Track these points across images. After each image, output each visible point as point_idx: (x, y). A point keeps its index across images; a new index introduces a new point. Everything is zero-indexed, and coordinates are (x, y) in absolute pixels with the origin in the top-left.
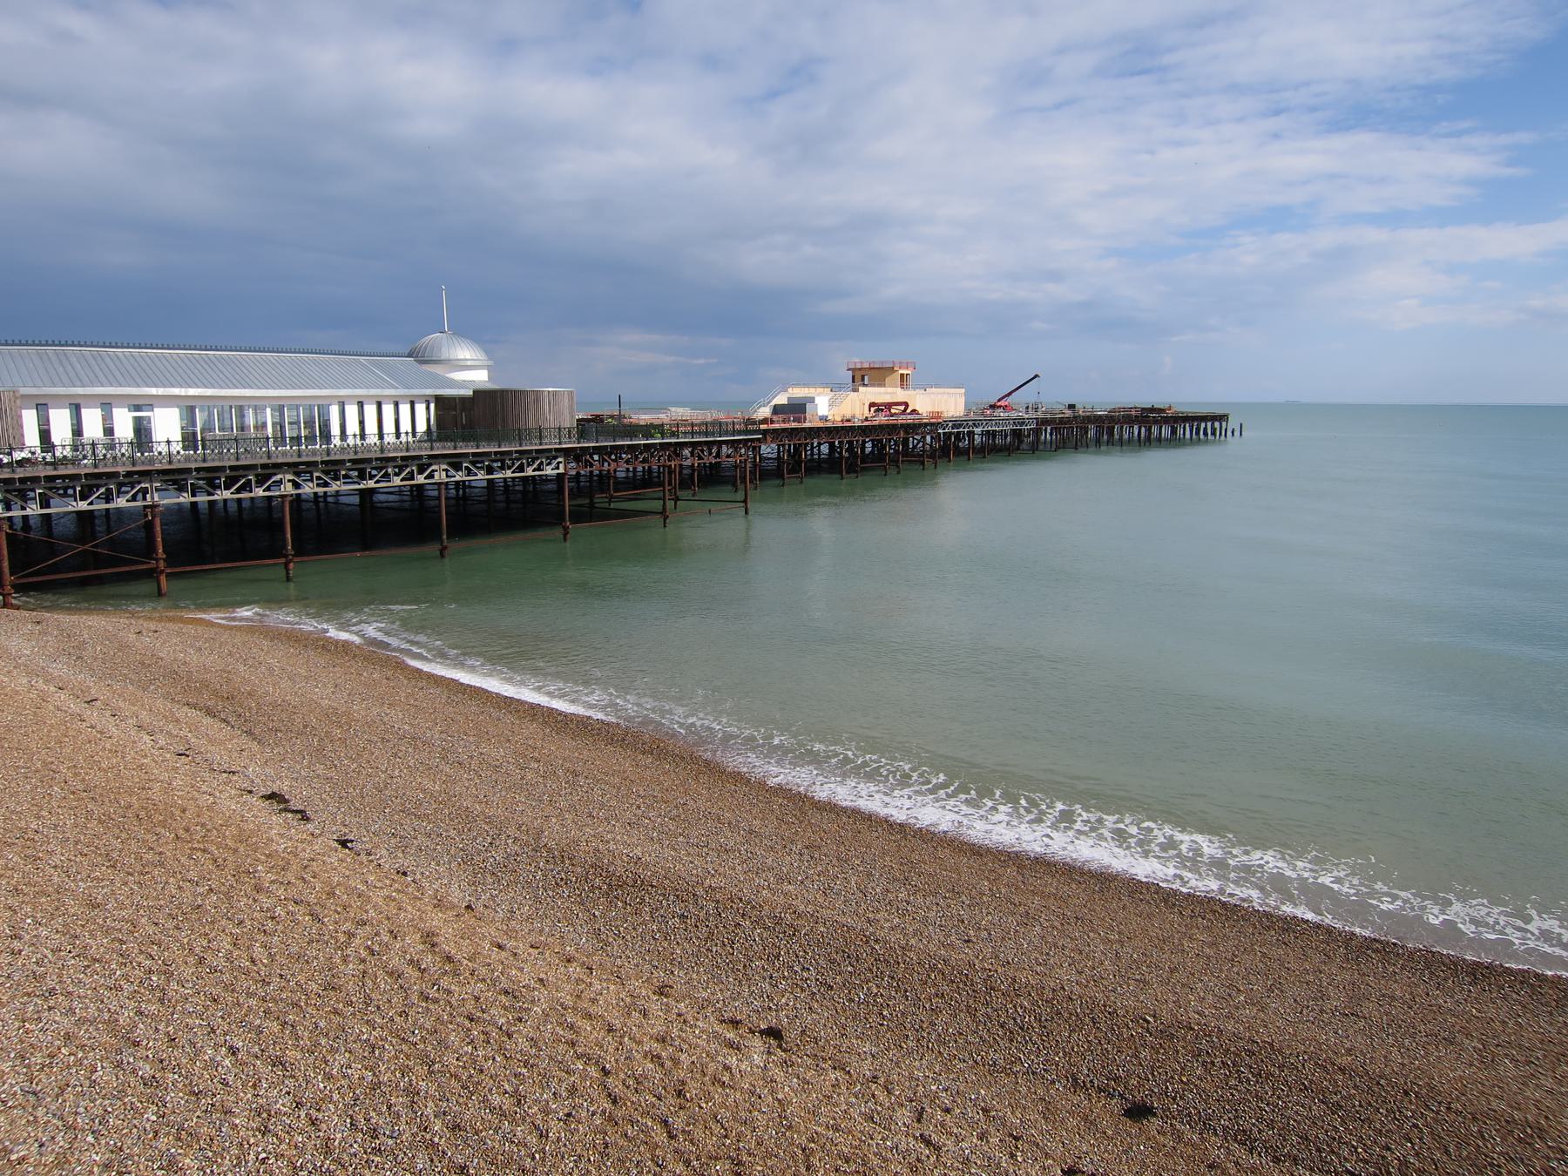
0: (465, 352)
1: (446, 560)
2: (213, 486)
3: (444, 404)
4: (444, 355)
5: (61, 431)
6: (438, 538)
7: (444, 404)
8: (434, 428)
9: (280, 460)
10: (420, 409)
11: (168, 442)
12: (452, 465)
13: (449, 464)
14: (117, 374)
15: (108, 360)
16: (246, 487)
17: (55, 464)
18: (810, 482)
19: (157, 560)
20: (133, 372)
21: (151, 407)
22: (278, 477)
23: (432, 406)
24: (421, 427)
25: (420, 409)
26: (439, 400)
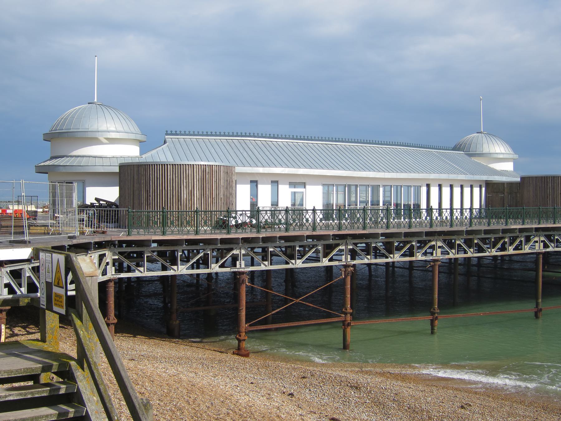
0: (499, 148)
1: (540, 321)
2: (389, 249)
3: (492, 188)
4: (486, 150)
5: (264, 202)
6: (537, 299)
7: (492, 188)
8: (484, 207)
9: (439, 229)
10: (476, 190)
11: (314, 210)
12: (548, 237)
13: (444, 241)
14: (221, 154)
15: (209, 144)
16: (205, 262)
17: (258, 227)
18: (360, 331)
19: (346, 314)
20: (273, 160)
21: (304, 185)
22: (433, 243)
23: (483, 189)
24: (476, 205)
25: (476, 190)
26: (489, 185)
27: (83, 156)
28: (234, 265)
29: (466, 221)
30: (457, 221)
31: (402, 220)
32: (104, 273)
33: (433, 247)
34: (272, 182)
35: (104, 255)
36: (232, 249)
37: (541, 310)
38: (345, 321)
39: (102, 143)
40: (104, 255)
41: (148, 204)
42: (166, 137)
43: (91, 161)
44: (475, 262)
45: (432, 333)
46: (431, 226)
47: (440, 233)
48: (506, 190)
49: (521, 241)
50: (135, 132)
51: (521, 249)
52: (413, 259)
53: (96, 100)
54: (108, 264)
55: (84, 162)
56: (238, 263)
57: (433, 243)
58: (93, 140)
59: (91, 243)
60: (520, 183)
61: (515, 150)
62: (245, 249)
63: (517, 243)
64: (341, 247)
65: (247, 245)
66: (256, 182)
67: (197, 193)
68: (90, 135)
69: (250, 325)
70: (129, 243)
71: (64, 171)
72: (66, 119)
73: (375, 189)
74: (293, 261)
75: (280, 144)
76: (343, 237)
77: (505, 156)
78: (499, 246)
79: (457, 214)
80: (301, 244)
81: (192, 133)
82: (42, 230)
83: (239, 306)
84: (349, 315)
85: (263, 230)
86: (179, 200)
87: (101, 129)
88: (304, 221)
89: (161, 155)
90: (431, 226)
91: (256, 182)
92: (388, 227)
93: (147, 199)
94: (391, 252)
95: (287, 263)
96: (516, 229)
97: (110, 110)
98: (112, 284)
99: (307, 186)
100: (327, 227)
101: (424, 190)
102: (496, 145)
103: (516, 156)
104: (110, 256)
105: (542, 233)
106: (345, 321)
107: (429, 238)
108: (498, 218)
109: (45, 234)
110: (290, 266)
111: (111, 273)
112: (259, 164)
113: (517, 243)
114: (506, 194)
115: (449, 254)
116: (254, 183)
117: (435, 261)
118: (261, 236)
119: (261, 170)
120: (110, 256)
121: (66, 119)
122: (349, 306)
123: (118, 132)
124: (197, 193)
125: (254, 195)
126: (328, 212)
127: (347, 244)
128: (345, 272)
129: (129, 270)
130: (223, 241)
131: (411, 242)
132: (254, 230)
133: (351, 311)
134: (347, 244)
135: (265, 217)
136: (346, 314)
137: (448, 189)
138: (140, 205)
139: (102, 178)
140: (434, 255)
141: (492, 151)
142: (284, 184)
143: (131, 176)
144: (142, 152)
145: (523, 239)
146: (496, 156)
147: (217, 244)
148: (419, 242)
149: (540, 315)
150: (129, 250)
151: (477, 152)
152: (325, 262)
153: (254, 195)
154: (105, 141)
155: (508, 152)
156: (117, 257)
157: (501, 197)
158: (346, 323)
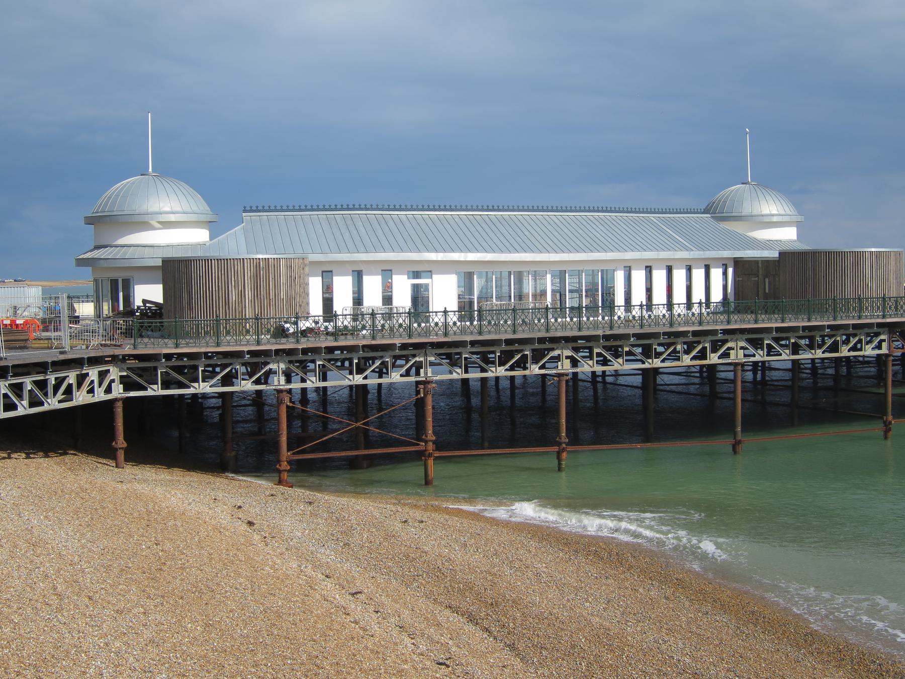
4: (747, 209)
8: (731, 297)
9: (559, 334)
10: (716, 274)
12: (751, 341)
15: (391, 224)
17: (338, 333)
19: (426, 442)
21: (429, 274)
22: (556, 353)
23: (730, 271)
24: (717, 296)
25: (716, 274)
26: (739, 264)
27: (130, 246)
28: (418, 374)
29: (693, 319)
30: (664, 321)
31: (568, 319)
32: (108, 390)
33: (558, 358)
34: (647, 267)
35: (108, 371)
36: (267, 363)
37: (740, 442)
38: (426, 450)
39: (154, 228)
40: (108, 371)
41: (191, 309)
42: (244, 214)
43: (138, 253)
44: (475, 386)
45: (886, 438)
46: (671, 325)
47: (567, 339)
48: (761, 271)
49: (704, 348)
50: (198, 211)
51: (861, 350)
52: (527, 372)
53: (150, 170)
54: (113, 381)
55: (129, 253)
56: (422, 371)
57: (556, 353)
58: (141, 224)
59: (83, 358)
60: (779, 261)
61: (797, 205)
62: (284, 362)
63: (853, 341)
64: (417, 359)
65: (570, 345)
66: (650, 267)
67: (249, 294)
68: (137, 219)
69: (294, 454)
70: (180, 356)
71: (106, 265)
72: (720, 201)
73: (520, 277)
74: (650, 361)
75: (493, 218)
76: (555, 340)
77: (786, 219)
78: (875, 343)
79: (679, 310)
80: (822, 333)
81: (315, 207)
82: (44, 344)
83: (279, 430)
84: (431, 444)
85: (343, 337)
86: (227, 302)
87: (151, 210)
88: (616, 318)
89: (236, 244)
90: (611, 328)
91: (650, 267)
92: (514, 332)
93: (190, 303)
94: (649, 357)
95: (451, 373)
96: (688, 332)
97: (172, 184)
98: (120, 405)
99: (434, 276)
100: (463, 331)
101: (620, 276)
102: (763, 202)
103: (800, 218)
104: (115, 373)
105: (741, 336)
106: (426, 450)
107: (726, 337)
108: (770, 314)
109: (48, 348)
110: (646, 366)
111: (118, 391)
112: (511, 249)
113: (853, 341)
114: (760, 276)
115: (781, 355)
116: (327, 276)
117: (559, 375)
118: (300, 347)
119: (363, 257)
120: (115, 373)
121: (720, 201)
122: (430, 432)
123: (184, 213)
124: (249, 294)
125: (328, 290)
126: (465, 308)
127: (426, 355)
128: (424, 389)
129: (182, 385)
130: (778, 329)
131: (522, 351)
132: (330, 338)
133: (434, 438)
134: (426, 355)
135: (345, 322)
136: (426, 442)
137: (702, 272)
138: (182, 309)
139: (146, 273)
140: (560, 367)
141: (755, 212)
142: (400, 273)
143: (176, 271)
144: (211, 238)
145: (707, 345)
146: (766, 219)
147: (534, 344)
148: (868, 335)
149: (739, 448)
150: (180, 363)
151: (733, 214)
152: (535, 370)
153: (328, 290)
154: (158, 226)
155: (783, 212)
156: (125, 374)
157: (762, 283)
158: (427, 453)
